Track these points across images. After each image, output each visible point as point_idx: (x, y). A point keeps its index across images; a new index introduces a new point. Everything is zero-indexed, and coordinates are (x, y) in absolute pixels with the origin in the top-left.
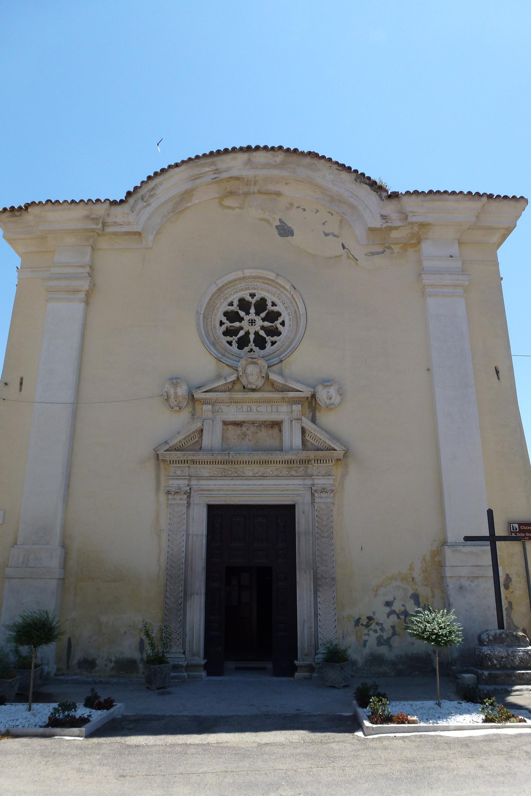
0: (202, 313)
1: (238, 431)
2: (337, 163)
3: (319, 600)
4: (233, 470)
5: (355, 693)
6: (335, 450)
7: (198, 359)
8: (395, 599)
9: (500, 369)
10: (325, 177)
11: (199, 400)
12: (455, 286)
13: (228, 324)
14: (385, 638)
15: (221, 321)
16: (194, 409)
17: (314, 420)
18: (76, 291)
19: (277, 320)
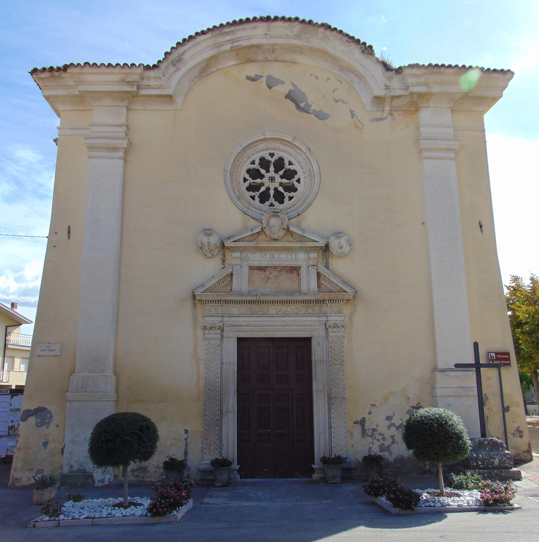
0: (229, 170)
1: (262, 274)
2: (347, 35)
3: (332, 415)
4: (259, 309)
5: (92, 434)
6: (346, 292)
7: (229, 214)
8: (394, 414)
9: (483, 224)
10: (336, 47)
11: (229, 248)
12: (448, 150)
13: (250, 180)
14: (386, 445)
15: (245, 178)
16: (224, 256)
17: (327, 266)
18: (115, 149)
19: (294, 178)
